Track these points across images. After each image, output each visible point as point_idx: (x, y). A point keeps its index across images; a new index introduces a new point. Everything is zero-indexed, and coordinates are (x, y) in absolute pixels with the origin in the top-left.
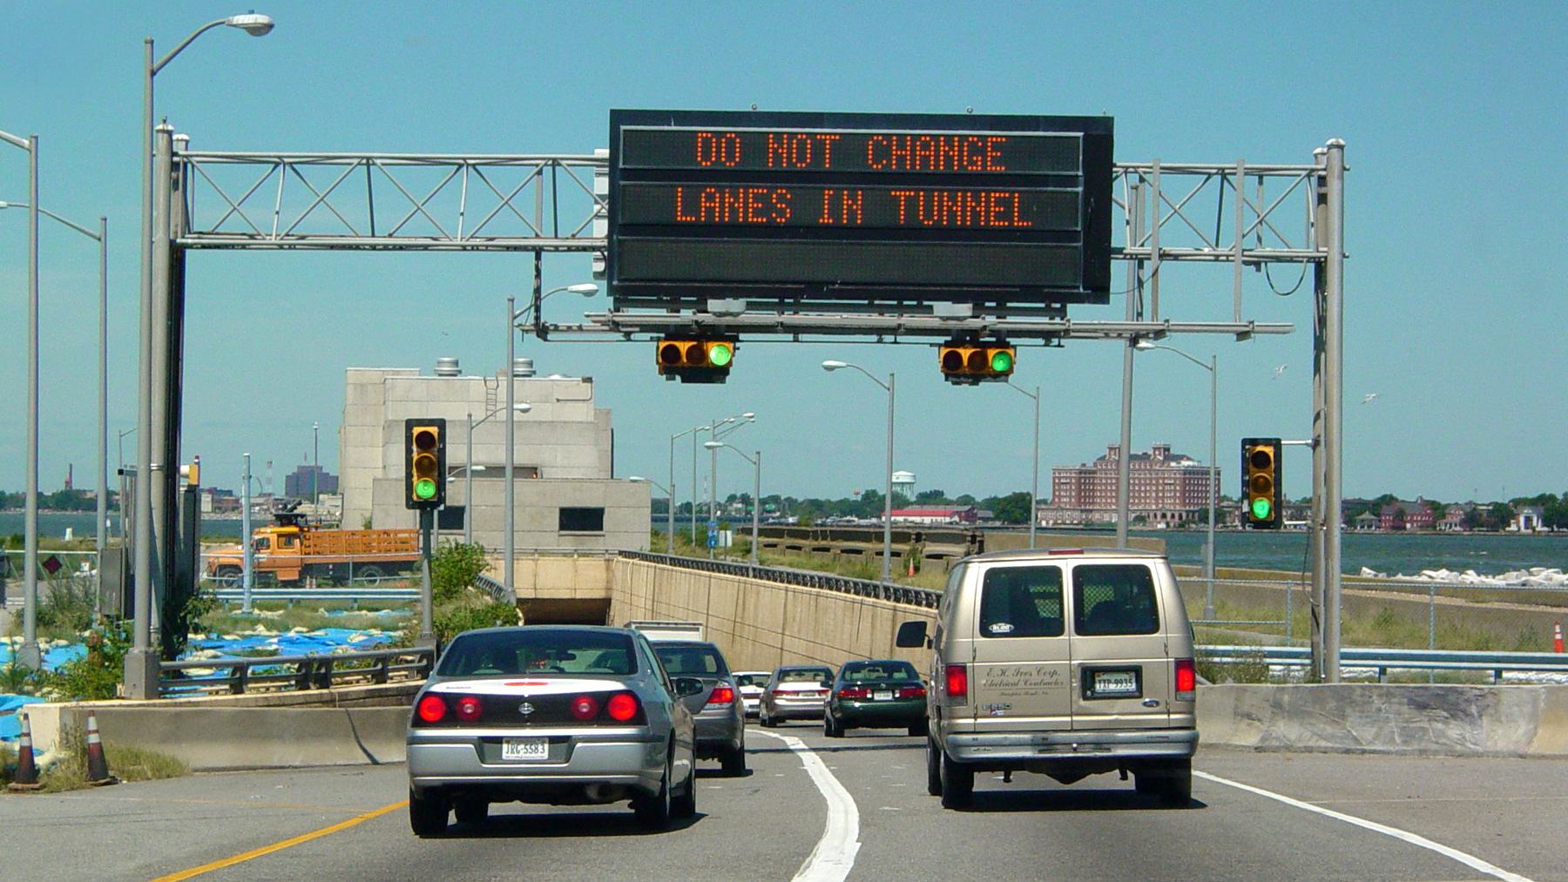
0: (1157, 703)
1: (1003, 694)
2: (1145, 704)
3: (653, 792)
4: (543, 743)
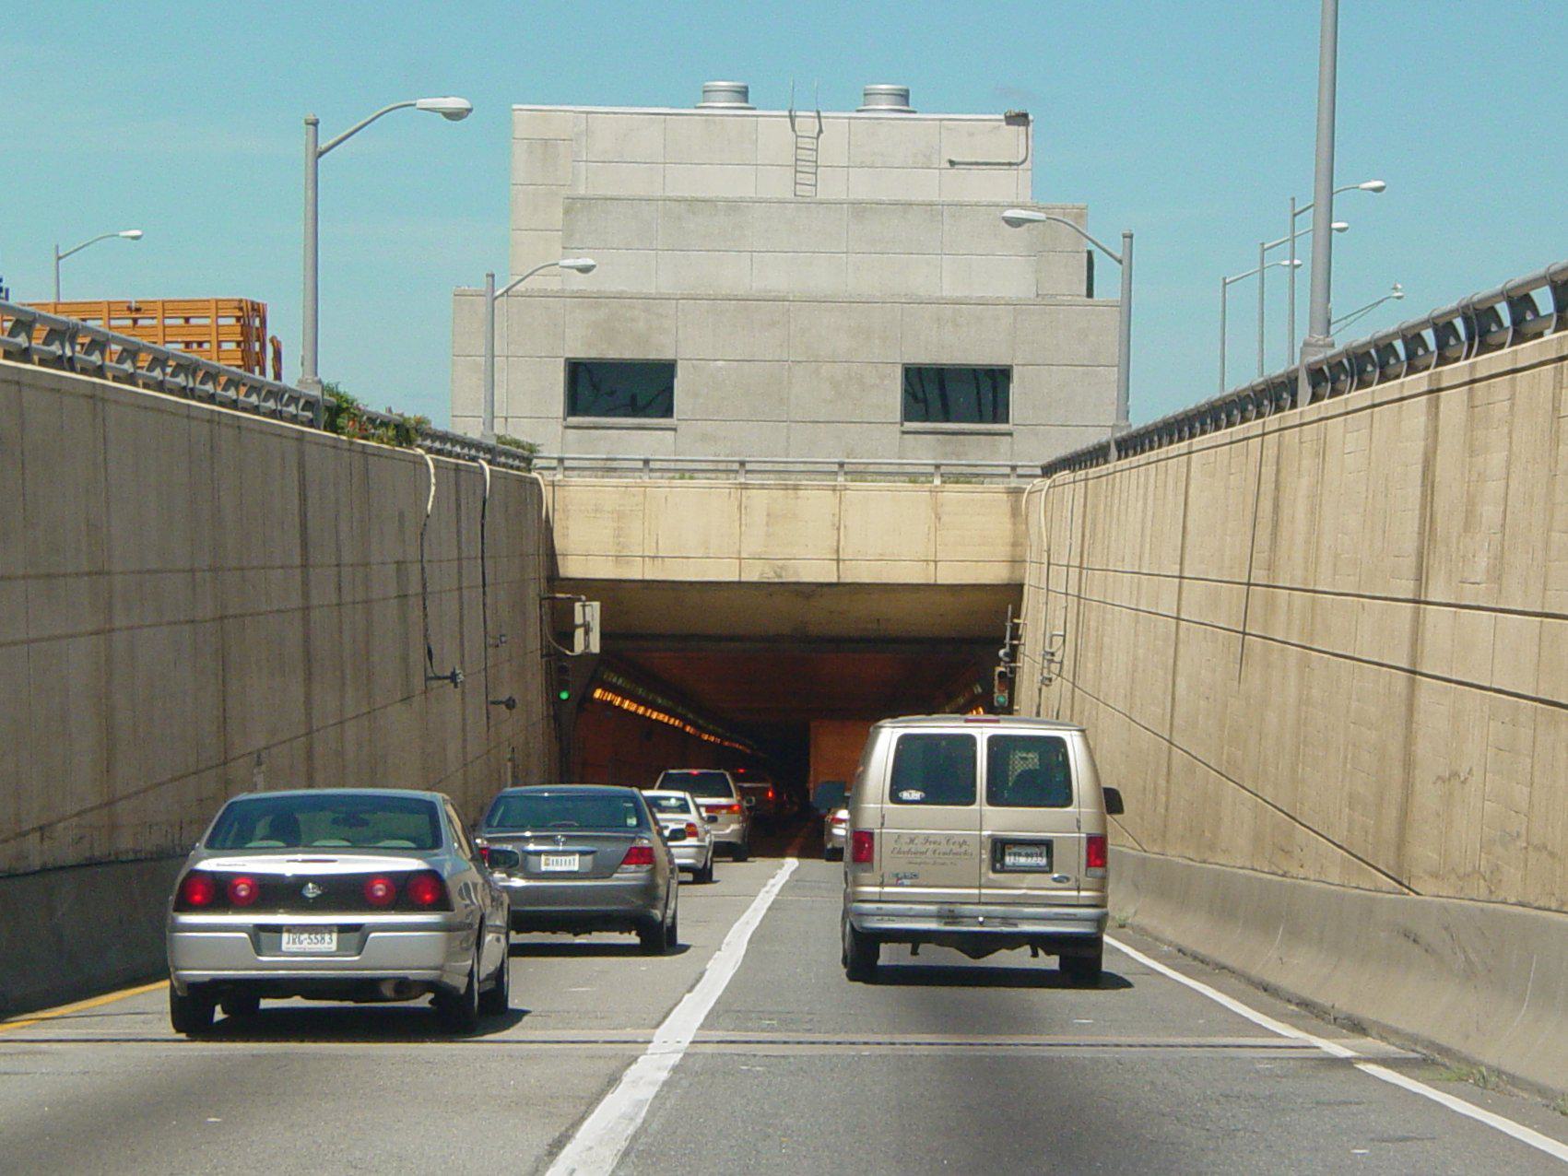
0: (1068, 879)
1: (910, 863)
2: (1055, 880)
3: (456, 989)
4: (330, 932)
